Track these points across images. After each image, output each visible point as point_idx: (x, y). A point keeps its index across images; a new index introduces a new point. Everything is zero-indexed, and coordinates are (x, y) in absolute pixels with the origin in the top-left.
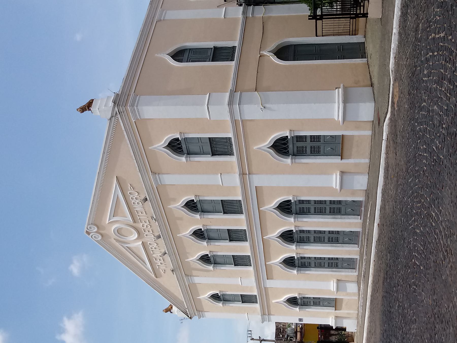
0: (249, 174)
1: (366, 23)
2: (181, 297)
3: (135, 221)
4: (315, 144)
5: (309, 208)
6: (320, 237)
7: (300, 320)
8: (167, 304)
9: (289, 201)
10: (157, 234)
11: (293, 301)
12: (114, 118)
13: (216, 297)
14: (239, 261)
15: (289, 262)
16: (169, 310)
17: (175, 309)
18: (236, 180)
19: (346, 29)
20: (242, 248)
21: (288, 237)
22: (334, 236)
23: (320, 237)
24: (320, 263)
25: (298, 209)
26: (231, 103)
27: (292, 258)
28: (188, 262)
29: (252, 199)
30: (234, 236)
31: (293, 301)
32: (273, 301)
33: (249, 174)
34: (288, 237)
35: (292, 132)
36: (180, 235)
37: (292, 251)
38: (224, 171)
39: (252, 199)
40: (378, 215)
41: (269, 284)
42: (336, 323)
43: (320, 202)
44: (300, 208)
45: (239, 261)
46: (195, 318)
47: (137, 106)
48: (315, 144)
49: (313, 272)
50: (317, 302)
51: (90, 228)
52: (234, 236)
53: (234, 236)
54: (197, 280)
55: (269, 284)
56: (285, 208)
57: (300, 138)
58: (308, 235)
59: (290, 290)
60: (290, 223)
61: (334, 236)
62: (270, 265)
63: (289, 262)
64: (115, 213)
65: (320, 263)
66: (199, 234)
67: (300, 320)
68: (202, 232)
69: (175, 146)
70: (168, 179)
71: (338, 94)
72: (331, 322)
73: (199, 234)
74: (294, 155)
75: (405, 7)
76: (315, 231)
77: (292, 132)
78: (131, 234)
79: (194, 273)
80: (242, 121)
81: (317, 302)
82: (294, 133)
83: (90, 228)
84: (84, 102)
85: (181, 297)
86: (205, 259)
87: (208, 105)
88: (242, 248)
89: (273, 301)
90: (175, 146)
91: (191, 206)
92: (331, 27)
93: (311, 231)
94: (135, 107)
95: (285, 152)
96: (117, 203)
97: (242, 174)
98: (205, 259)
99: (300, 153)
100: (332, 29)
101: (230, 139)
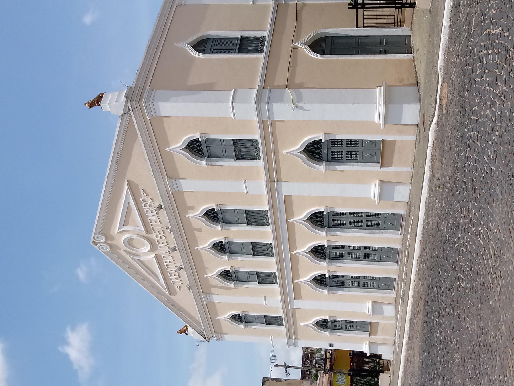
2: (198, 317)
6: (354, 254)
7: (331, 345)
8: (182, 324)
10: (172, 246)
11: (323, 324)
13: (236, 318)
14: (264, 278)
16: (184, 331)
17: (190, 330)
20: (268, 264)
21: (319, 252)
23: (354, 254)
24: (354, 282)
28: (198, 251)
30: (258, 250)
31: (323, 324)
32: (301, 324)
34: (319, 252)
39: (280, 212)
40: (402, 377)
41: (297, 304)
45: (264, 278)
46: (213, 341)
48: (352, 149)
49: (346, 292)
50: (350, 326)
52: (258, 250)
54: (216, 298)
55: (297, 304)
59: (320, 312)
62: (298, 284)
63: (320, 281)
64: (125, 222)
65: (354, 282)
66: (220, 247)
67: (331, 345)
69: (195, 148)
71: (379, 93)
72: (365, 348)
73: (220, 247)
74: (328, 161)
75: (456, 6)
78: (143, 245)
79: (213, 290)
80: (271, 121)
81: (350, 326)
83: (97, 237)
85: (198, 317)
88: (268, 264)
89: (284, 152)
90: (195, 148)
91: (212, 215)
94: (150, 103)
96: (128, 211)
98: (226, 275)
99: (335, 159)
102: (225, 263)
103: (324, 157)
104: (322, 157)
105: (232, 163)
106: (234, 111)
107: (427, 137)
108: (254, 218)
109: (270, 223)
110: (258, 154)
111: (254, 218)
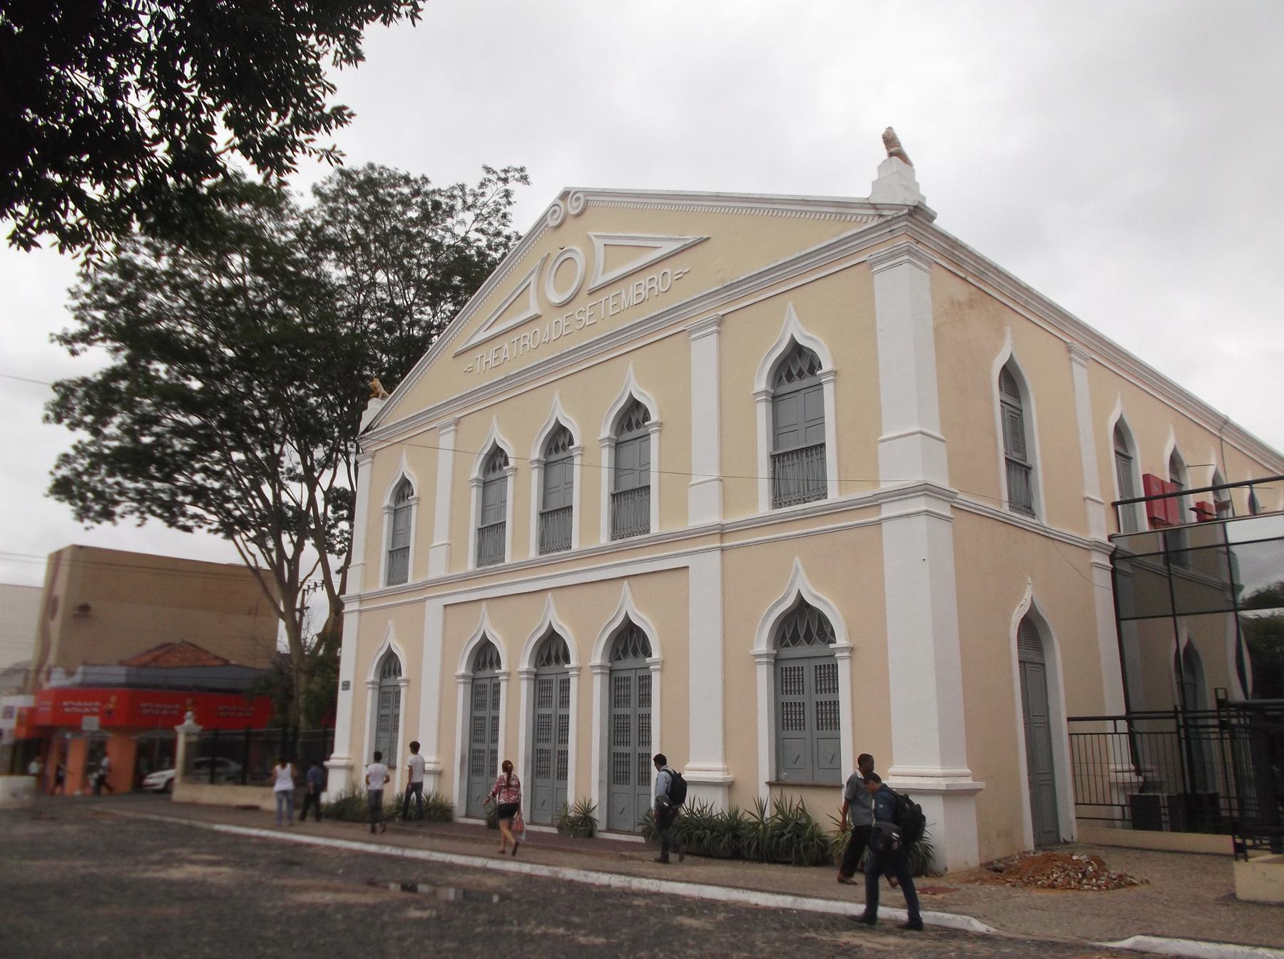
0: (723, 550)
1: (1120, 847)
3: (591, 293)
4: (810, 715)
5: (627, 702)
9: (567, 660)
11: (389, 665)
12: (872, 212)
14: (491, 534)
15: (485, 655)
18: (704, 513)
19: (1086, 794)
20: (522, 538)
21: (551, 650)
22: (554, 767)
25: (481, 682)
26: (926, 490)
27: (397, 671)
29: (666, 557)
30: (555, 516)
31: (389, 665)
33: (723, 550)
34: (551, 650)
35: (847, 654)
36: (557, 398)
37: (516, 660)
38: (730, 483)
39: (666, 557)
42: (861, 903)
43: (564, 729)
44: (551, 681)
45: (491, 534)
47: (909, 262)
48: (810, 715)
51: (578, 199)
52: (555, 516)
53: (554, 521)
56: (629, 641)
57: (828, 676)
58: (634, 699)
60: (588, 655)
61: (554, 767)
63: (485, 655)
66: (559, 440)
67: (346, 685)
68: (564, 448)
69: (796, 365)
70: (704, 351)
73: (559, 440)
74: (611, 671)
76: (496, 718)
77: (847, 654)
78: (559, 290)
80: (878, 523)
82: (842, 658)
83: (578, 199)
84: (907, 148)
86: (496, 459)
87: (922, 433)
88: (522, 538)
89: (797, 560)
90: (796, 365)
91: (632, 416)
92: (1097, 755)
93: (650, 706)
94: (906, 257)
95: (784, 636)
97: (722, 531)
98: (496, 459)
99: (785, 678)
100: (1083, 759)
101: (825, 496)
102: (525, 452)
103: (789, 652)
104: (787, 645)
105: (473, 523)
106: (906, 435)
107: (808, 892)
108: (629, 500)
109: (619, 541)
110: (780, 506)
111: (629, 500)
